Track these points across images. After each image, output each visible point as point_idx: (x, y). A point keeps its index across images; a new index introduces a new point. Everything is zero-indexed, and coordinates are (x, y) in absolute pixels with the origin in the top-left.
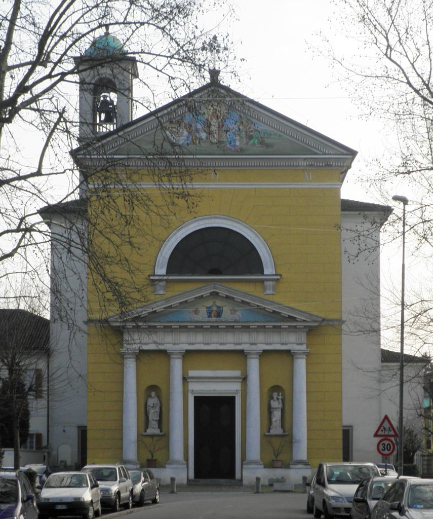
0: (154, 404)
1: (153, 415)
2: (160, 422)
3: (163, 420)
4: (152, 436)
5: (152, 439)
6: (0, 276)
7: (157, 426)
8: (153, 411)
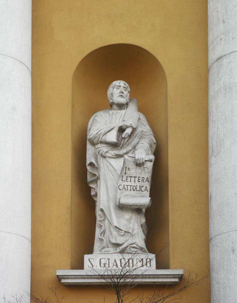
0: (121, 130)
1: (119, 185)
2: (154, 219)
3: (146, 278)
4: (116, 286)
5: (115, 297)
6: (117, 302)
7: (140, 239)
8: (118, 164)
